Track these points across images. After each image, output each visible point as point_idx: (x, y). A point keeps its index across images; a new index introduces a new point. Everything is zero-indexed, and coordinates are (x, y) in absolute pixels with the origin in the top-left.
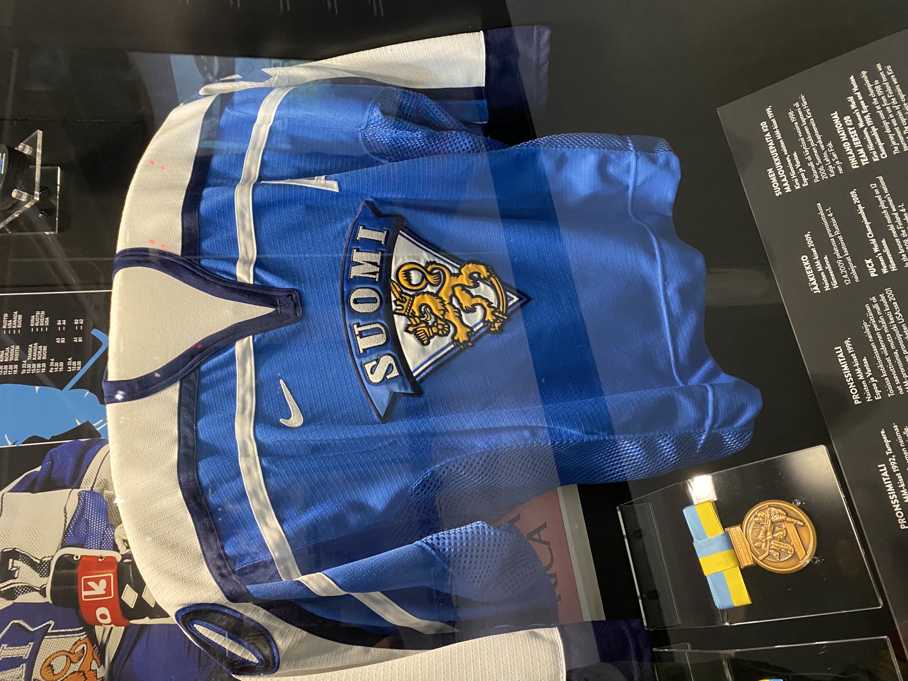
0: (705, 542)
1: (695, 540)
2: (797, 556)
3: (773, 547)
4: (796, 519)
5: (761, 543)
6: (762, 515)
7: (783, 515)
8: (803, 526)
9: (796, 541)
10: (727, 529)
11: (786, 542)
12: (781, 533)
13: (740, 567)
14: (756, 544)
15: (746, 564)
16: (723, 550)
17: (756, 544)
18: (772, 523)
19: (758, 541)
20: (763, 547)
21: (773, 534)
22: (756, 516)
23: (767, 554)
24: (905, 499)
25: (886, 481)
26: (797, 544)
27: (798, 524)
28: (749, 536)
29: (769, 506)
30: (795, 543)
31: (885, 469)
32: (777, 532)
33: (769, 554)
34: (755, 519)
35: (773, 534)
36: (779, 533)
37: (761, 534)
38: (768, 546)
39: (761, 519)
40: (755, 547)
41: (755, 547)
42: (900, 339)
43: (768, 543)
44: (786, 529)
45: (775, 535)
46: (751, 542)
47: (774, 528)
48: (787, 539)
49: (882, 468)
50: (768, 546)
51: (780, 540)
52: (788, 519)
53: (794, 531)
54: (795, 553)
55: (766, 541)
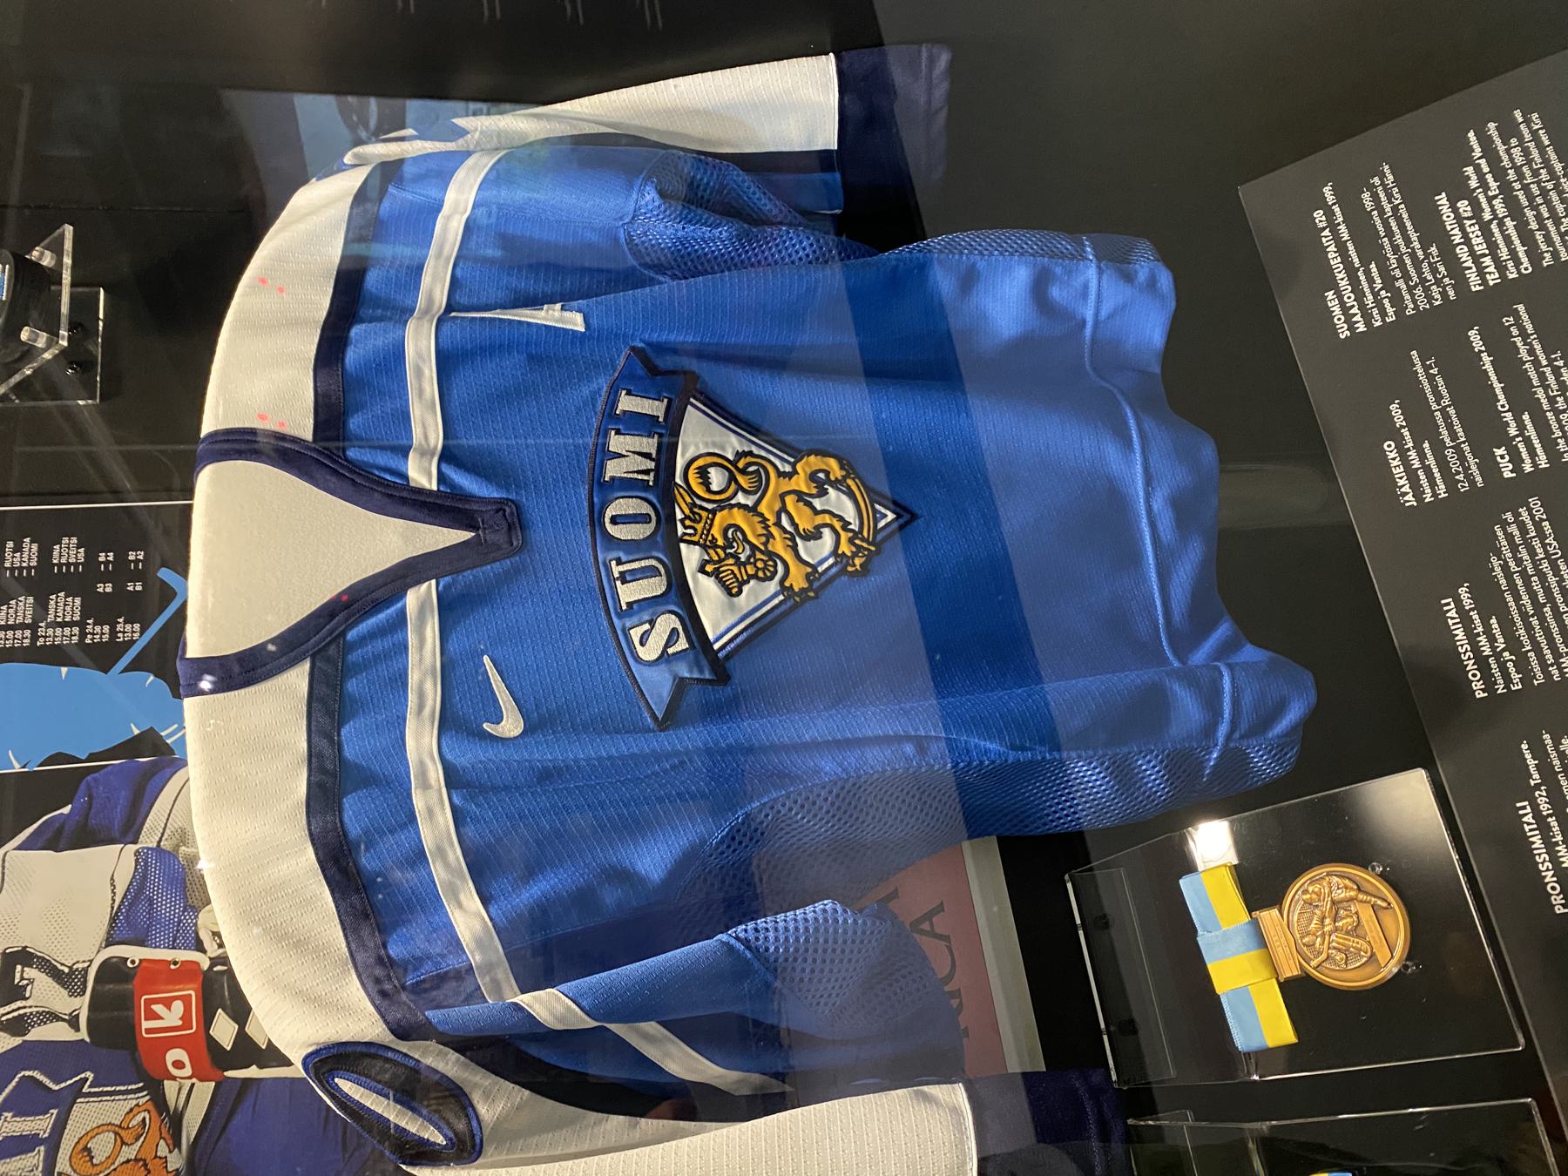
0: (1217, 936)
1: (1200, 932)
2: (1377, 960)
3: (1334, 944)
4: (1375, 896)
5: (1314, 937)
6: (1316, 890)
7: (1352, 889)
9: (1374, 934)
11: (1358, 936)
12: (1349, 920)
13: (1277, 979)
14: (1306, 940)
15: (1289, 975)
16: (1249, 950)
17: (1306, 940)
19: (1308, 934)
20: (1317, 945)
21: (1335, 922)
22: (1306, 892)
23: (1324, 956)
24: (1563, 862)
25: (1531, 830)
28: (1293, 925)
29: (1328, 874)
30: (1373, 937)
31: (1529, 809)
33: (1328, 957)
34: (1305, 897)
35: (1335, 922)
36: (1344, 921)
37: (1315, 922)
39: (1314, 896)
40: (1304, 944)
41: (1304, 944)
42: (1554, 585)
43: (1327, 937)
44: (1357, 913)
45: (1339, 924)
46: (1298, 936)
47: (1337, 913)
48: (1360, 931)
50: (1326, 942)
51: (1347, 933)
52: (1361, 896)
53: (1371, 916)
54: (1373, 954)
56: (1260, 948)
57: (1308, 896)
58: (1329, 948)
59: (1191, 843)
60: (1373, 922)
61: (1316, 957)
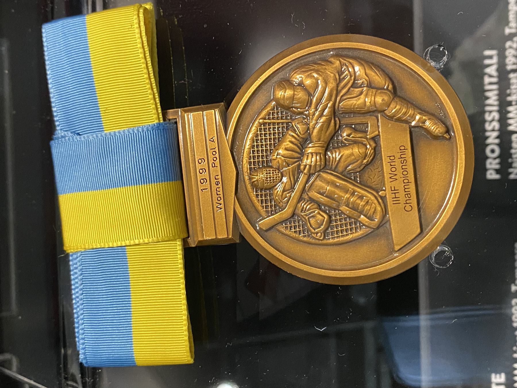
0: (88, 143)
1: (59, 132)
2: (388, 234)
3: (314, 194)
4: (423, 111)
5: (277, 175)
6: (308, 82)
7: (379, 89)
8: (436, 138)
9: (399, 185)
10: (171, 113)
11: (364, 185)
12: (356, 150)
13: (185, 242)
14: (260, 176)
15: (209, 236)
16: (144, 180)
17: (260, 176)
18: (334, 112)
19: (267, 165)
20: (279, 188)
21: (326, 150)
22: (287, 83)
23: (287, 212)
24: (510, 125)
25: (491, 84)
26: (401, 195)
27: (427, 131)
28: (242, 145)
29: (340, 54)
30: (395, 191)
31: (495, 60)
32: (343, 145)
33: (293, 214)
34: (280, 94)
35: (326, 150)
36: (346, 152)
37: (287, 144)
38: (298, 187)
39: (301, 95)
40: (254, 185)
41: (254, 185)
42: (165, 136)
43: (302, 178)
44: (375, 139)
45: (335, 155)
46: (246, 166)
47: (336, 132)
48: (371, 176)
49: (490, 57)
50: (298, 187)
51: (345, 176)
52: (394, 108)
53: (402, 151)
54: (384, 222)
55: (298, 171)
56: (167, 178)
57: (289, 93)
58: (300, 199)
59: (83, 9)
60: (404, 161)
61: (270, 213)
